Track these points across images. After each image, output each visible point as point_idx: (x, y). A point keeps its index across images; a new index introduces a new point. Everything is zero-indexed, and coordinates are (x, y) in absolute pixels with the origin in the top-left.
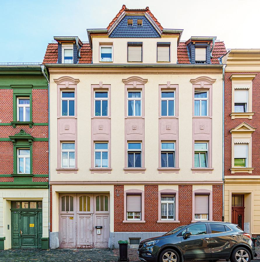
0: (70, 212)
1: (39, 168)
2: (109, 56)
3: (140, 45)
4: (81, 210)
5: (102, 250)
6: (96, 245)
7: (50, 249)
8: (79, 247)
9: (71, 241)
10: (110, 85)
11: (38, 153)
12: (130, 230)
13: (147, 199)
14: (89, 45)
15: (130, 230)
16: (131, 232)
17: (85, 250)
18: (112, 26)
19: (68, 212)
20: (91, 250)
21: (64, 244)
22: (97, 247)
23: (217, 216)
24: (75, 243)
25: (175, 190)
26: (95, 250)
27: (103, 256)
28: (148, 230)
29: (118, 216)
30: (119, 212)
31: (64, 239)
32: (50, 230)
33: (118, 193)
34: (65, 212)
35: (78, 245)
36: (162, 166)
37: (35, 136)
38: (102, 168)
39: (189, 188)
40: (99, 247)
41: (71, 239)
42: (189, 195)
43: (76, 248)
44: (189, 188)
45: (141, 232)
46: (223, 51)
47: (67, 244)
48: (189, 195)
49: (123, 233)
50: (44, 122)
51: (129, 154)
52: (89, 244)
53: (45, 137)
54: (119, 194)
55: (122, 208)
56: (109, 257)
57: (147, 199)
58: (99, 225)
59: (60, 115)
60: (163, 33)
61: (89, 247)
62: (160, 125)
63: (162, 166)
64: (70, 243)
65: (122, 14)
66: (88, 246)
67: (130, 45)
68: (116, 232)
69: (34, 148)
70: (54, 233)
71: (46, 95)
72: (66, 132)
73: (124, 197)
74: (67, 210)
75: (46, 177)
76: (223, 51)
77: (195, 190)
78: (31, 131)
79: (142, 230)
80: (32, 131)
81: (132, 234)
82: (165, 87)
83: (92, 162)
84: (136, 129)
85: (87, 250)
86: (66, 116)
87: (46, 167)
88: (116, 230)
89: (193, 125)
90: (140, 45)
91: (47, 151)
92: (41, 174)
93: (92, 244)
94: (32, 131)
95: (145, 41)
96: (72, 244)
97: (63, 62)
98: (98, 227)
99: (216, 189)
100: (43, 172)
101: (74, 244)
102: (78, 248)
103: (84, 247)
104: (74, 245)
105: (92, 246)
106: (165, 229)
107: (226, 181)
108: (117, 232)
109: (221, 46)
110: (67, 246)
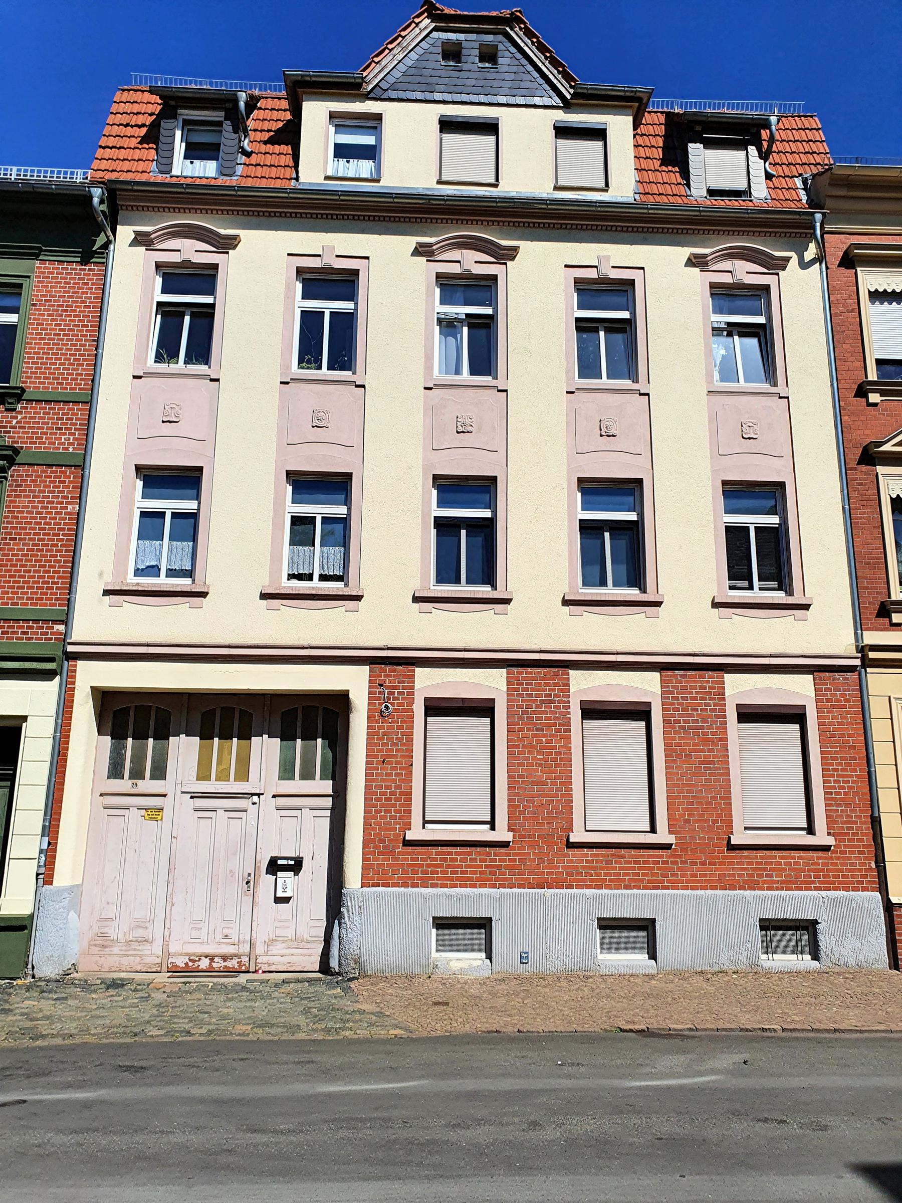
0: (147, 785)
1: (24, 577)
2: (370, 153)
3: (491, 128)
4: (203, 774)
5: (298, 981)
6: (266, 954)
7: (33, 977)
8: (181, 962)
9: (140, 933)
10: (368, 258)
11: (28, 512)
12: (439, 879)
13: (521, 730)
14: (285, 104)
15: (439, 879)
16: (443, 886)
17: (209, 982)
18: (383, 63)
19: (140, 782)
20: (242, 979)
21: (104, 947)
22: (273, 968)
23: (847, 816)
24: (159, 942)
25: (646, 692)
26: (262, 982)
27: (306, 1011)
28: (526, 880)
29: (382, 805)
30: (387, 787)
31: (106, 920)
32: (46, 875)
33: (389, 699)
34: (124, 784)
35: (176, 954)
36: (440, 580)
37: (26, 443)
38: (321, 589)
39: (708, 682)
40: (279, 963)
41: (140, 924)
42: (710, 716)
43: (164, 969)
44: (708, 682)
45: (494, 886)
46: (815, 153)
47: (116, 950)
48: (710, 716)
49: (404, 894)
50: (76, 387)
51: (579, 329)
52: (231, 950)
53: (71, 450)
54: (393, 704)
55: (401, 769)
56: (338, 1015)
57: (521, 730)
58: (289, 851)
59: (146, 363)
60: (574, 96)
61: (233, 964)
62: (573, 415)
63: (440, 580)
64: (135, 945)
65: (422, 26)
66: (225, 958)
67: (448, 125)
68: (373, 886)
69: (16, 491)
70: (60, 891)
71: (92, 284)
72: (167, 429)
73: (412, 717)
74: (138, 774)
75: (56, 622)
76: (815, 150)
77: (736, 691)
78: (10, 422)
79: (497, 879)
80: (14, 421)
81: (450, 897)
82: (592, 274)
83: (276, 560)
84: (469, 429)
85: (222, 980)
86: (173, 368)
87: (59, 578)
88: (372, 878)
89: (714, 419)
90: (491, 128)
91: (70, 507)
92: (22, 604)
93: (246, 948)
94: (14, 421)
95: (507, 117)
96: (146, 949)
97: (176, 171)
98: (284, 862)
99: (830, 690)
100: (41, 599)
101: (157, 949)
102: (174, 971)
103: (204, 964)
104: (152, 954)
105: (245, 959)
106: (609, 874)
107: (872, 655)
108: (378, 885)
109: (807, 131)
110: (116, 959)
